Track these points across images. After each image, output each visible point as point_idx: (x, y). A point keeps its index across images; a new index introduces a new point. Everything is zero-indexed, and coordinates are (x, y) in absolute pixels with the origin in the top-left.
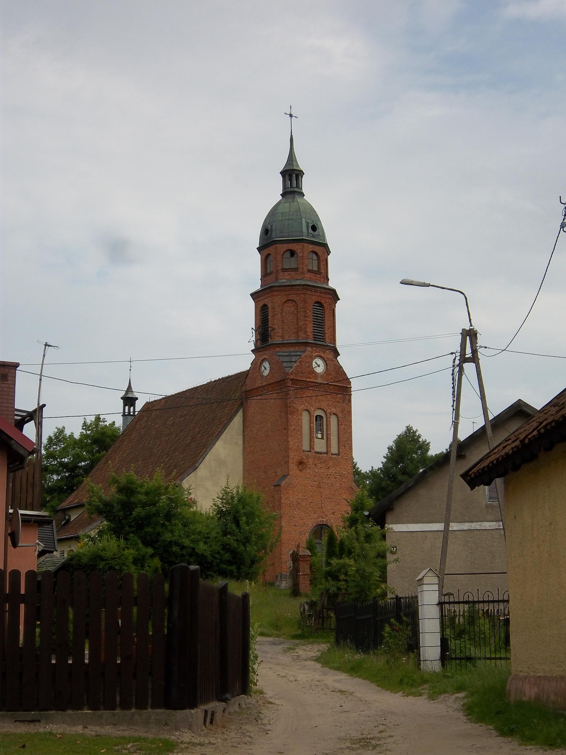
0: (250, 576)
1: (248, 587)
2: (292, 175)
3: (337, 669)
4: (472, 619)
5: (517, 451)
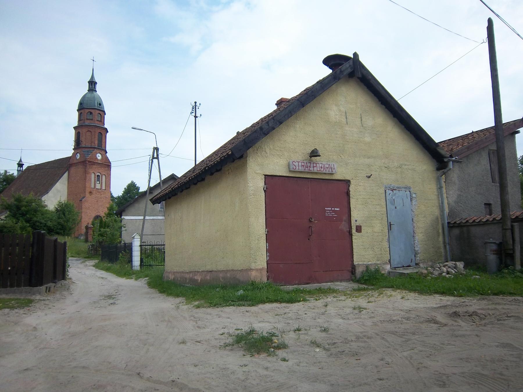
0: (68, 235)
1: (68, 240)
2: (92, 84)
3: (102, 269)
4: (152, 250)
5: (170, 192)
